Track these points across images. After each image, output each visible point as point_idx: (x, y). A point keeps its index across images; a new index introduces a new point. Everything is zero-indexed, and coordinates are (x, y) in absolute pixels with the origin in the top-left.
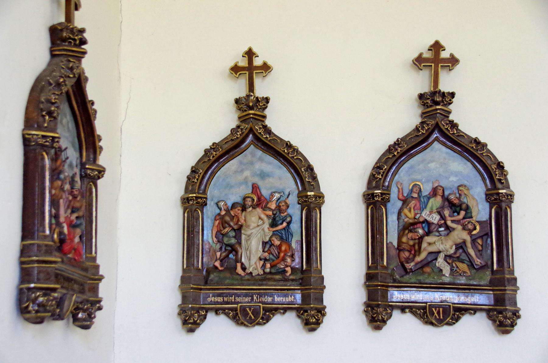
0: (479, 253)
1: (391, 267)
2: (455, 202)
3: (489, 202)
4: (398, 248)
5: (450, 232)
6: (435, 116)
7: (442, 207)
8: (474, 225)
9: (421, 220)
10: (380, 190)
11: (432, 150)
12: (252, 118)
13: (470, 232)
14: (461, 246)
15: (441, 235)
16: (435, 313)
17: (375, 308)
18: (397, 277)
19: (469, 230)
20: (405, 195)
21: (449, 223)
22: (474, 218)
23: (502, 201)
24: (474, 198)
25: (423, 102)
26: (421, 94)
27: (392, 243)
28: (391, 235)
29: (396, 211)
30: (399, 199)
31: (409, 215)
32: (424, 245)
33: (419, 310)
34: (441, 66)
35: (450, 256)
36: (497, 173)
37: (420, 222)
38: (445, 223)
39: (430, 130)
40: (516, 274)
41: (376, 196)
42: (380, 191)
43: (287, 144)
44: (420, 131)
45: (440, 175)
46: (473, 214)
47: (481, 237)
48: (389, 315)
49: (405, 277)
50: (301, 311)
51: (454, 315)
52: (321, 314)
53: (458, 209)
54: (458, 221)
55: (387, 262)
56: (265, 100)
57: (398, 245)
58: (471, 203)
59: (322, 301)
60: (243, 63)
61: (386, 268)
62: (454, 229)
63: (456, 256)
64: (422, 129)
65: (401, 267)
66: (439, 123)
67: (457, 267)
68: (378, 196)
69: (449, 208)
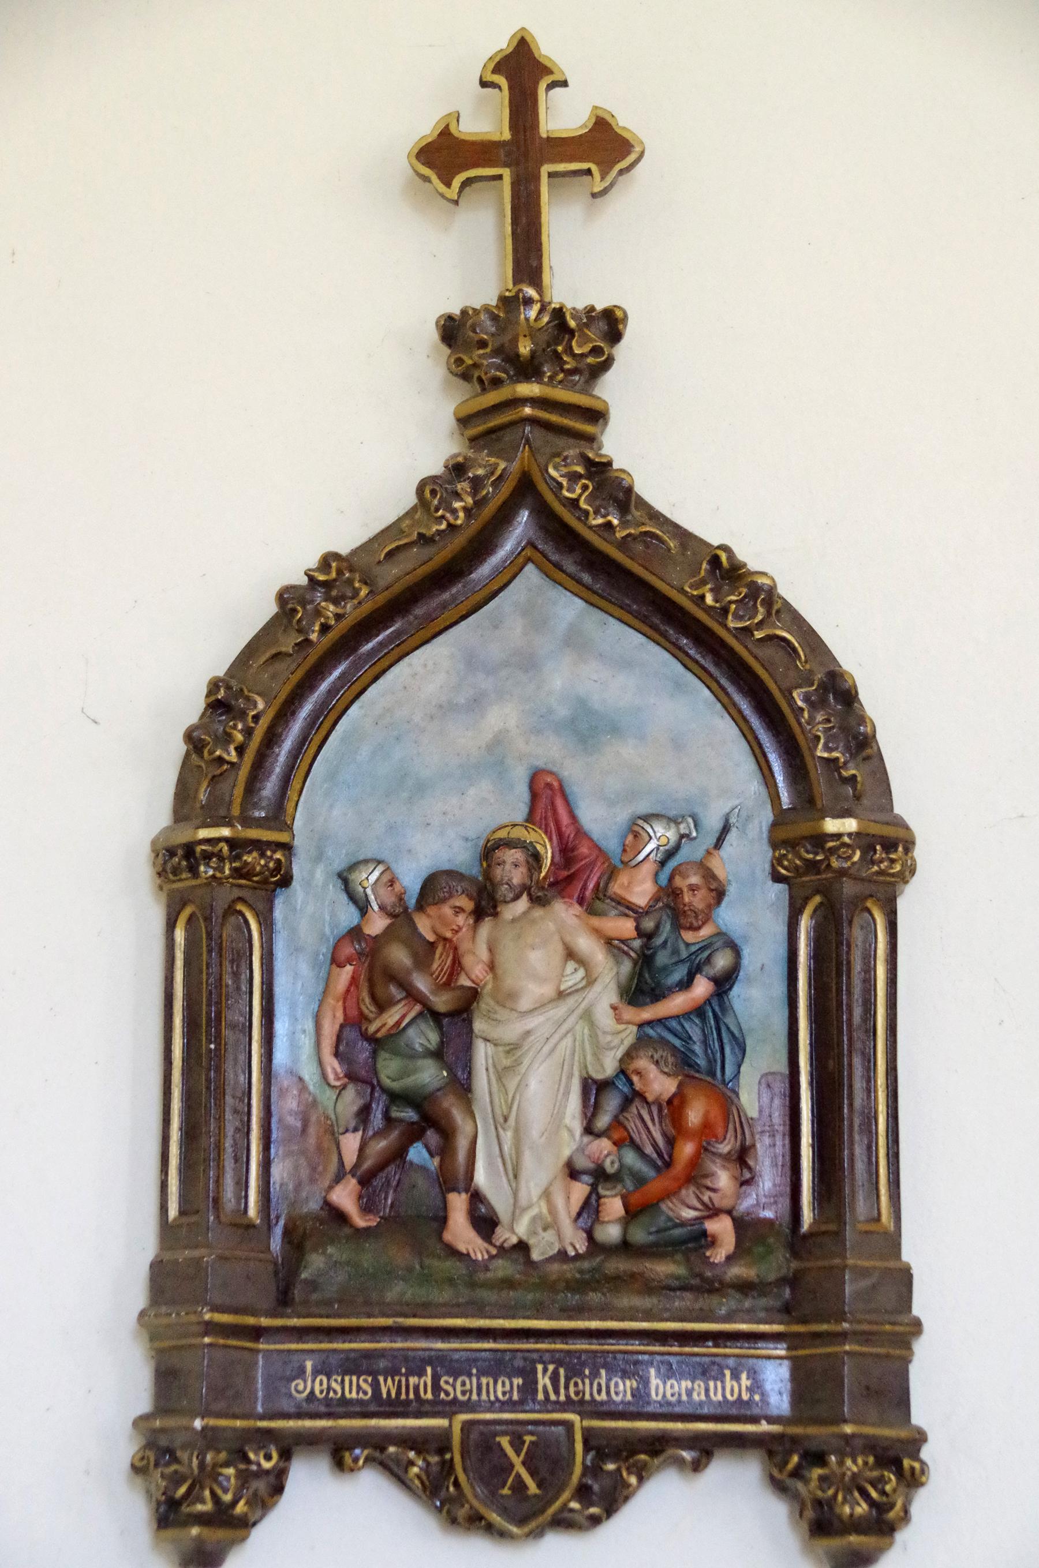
12: (533, 421)
25: (459, 361)
26: (450, 318)
34: (551, 175)
39: (489, 510)
43: (715, 561)
50: (791, 1459)
52: (900, 1473)
56: (603, 325)
59: (900, 1400)
60: (485, 120)
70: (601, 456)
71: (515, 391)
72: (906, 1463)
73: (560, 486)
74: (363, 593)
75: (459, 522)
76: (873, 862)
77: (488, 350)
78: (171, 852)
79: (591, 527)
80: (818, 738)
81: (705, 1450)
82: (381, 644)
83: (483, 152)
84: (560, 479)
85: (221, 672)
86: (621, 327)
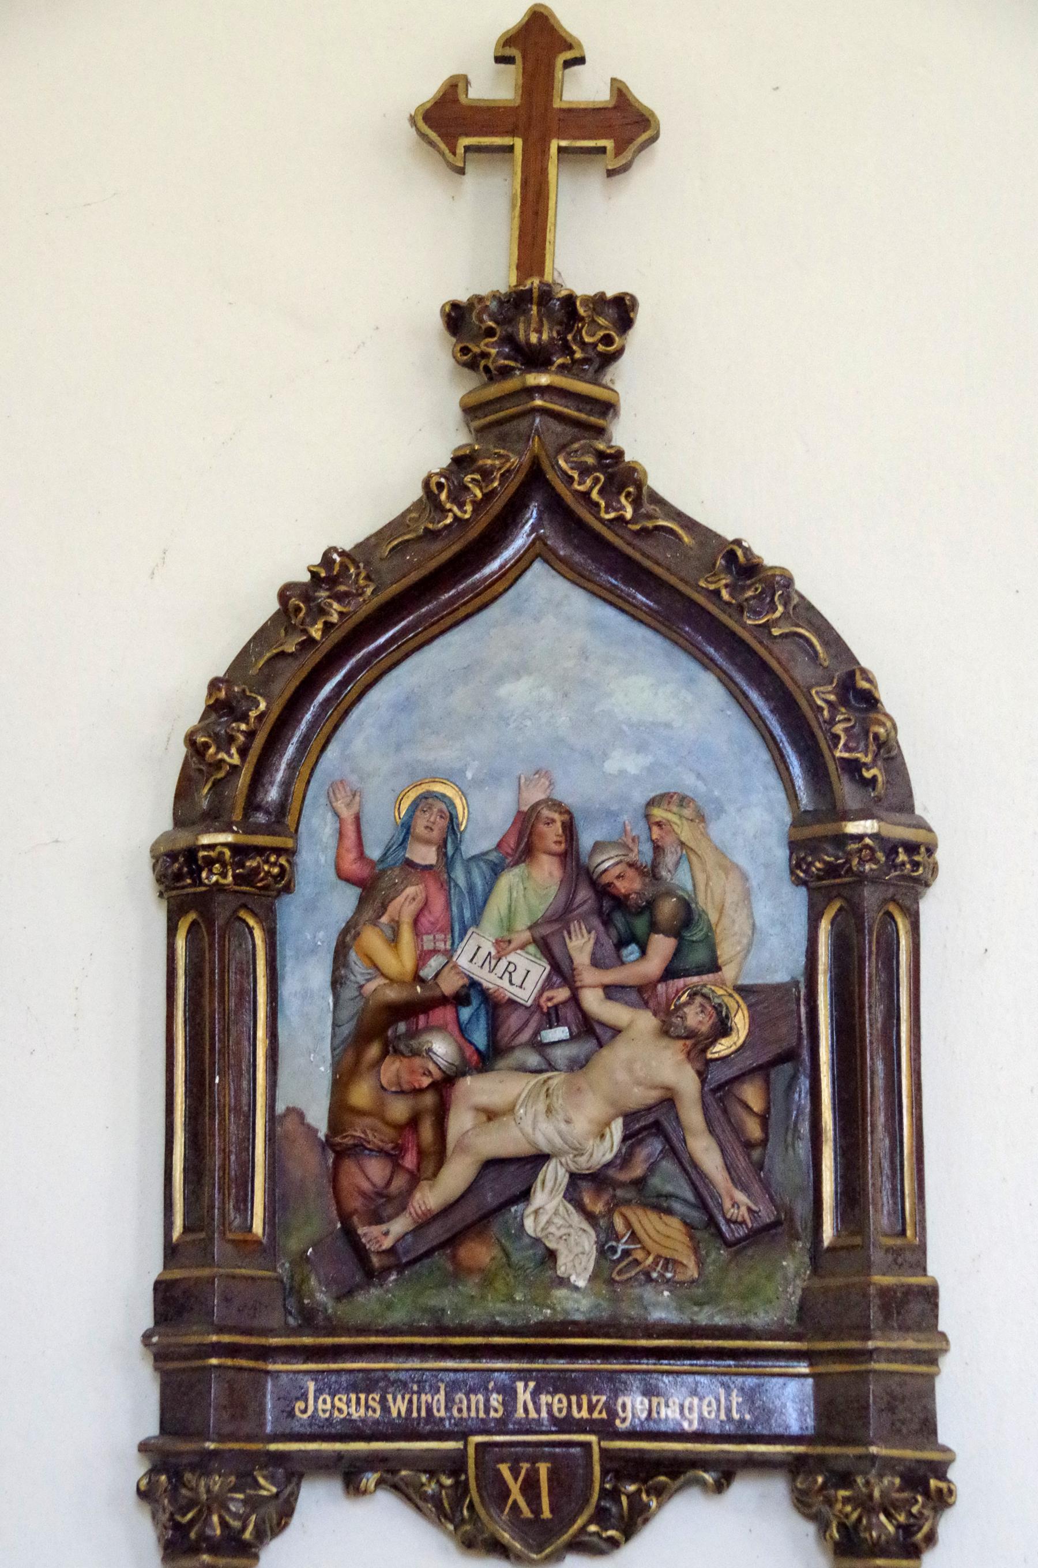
0: (749, 1158)
1: (294, 1244)
2: (622, 887)
3: (804, 883)
4: (329, 1144)
5: (601, 1045)
6: (523, 425)
7: (562, 917)
8: (718, 1008)
9: (449, 985)
10: (227, 828)
11: (517, 611)
13: (697, 1045)
15: (551, 1067)
16: (515, 1488)
17: (188, 1476)
18: (321, 1297)
19: (691, 1034)
20: (374, 853)
21: (593, 1001)
22: (729, 973)
23: (861, 878)
24: (728, 866)
25: (465, 350)
26: (455, 306)
27: (301, 1115)
28: (303, 1076)
29: (327, 939)
30: (341, 875)
31: (391, 959)
32: (461, 1121)
33: (432, 1474)
34: (560, 149)
35: (597, 1179)
36: (839, 729)
37: (443, 1000)
38: (575, 999)
39: (497, 506)
40: (938, 1266)
41: (210, 862)
42: (228, 838)
43: (731, 556)
44: (444, 511)
46: (725, 951)
47: (763, 1070)
48: (271, 1511)
49: (360, 1298)
51: (614, 1495)
52: (927, 1494)
53: (640, 925)
54: (640, 989)
55: (270, 1220)
58: (713, 894)
59: (928, 1427)
60: (493, 86)
61: (267, 1250)
62: (616, 1031)
63: (624, 1176)
64: (454, 498)
65: (341, 1244)
66: (545, 464)
67: (634, 1237)
68: (220, 859)
69: (596, 922)
70: (612, 447)
71: (524, 382)
72: (933, 1483)
73: (571, 478)
74: (369, 591)
75: (467, 516)
76: (895, 867)
77: (495, 339)
78: (173, 856)
79: (602, 521)
80: (837, 738)
81: (726, 1474)
82: (313, 725)
83: (488, 118)
84: (570, 472)
85: (221, 673)
86: (632, 315)
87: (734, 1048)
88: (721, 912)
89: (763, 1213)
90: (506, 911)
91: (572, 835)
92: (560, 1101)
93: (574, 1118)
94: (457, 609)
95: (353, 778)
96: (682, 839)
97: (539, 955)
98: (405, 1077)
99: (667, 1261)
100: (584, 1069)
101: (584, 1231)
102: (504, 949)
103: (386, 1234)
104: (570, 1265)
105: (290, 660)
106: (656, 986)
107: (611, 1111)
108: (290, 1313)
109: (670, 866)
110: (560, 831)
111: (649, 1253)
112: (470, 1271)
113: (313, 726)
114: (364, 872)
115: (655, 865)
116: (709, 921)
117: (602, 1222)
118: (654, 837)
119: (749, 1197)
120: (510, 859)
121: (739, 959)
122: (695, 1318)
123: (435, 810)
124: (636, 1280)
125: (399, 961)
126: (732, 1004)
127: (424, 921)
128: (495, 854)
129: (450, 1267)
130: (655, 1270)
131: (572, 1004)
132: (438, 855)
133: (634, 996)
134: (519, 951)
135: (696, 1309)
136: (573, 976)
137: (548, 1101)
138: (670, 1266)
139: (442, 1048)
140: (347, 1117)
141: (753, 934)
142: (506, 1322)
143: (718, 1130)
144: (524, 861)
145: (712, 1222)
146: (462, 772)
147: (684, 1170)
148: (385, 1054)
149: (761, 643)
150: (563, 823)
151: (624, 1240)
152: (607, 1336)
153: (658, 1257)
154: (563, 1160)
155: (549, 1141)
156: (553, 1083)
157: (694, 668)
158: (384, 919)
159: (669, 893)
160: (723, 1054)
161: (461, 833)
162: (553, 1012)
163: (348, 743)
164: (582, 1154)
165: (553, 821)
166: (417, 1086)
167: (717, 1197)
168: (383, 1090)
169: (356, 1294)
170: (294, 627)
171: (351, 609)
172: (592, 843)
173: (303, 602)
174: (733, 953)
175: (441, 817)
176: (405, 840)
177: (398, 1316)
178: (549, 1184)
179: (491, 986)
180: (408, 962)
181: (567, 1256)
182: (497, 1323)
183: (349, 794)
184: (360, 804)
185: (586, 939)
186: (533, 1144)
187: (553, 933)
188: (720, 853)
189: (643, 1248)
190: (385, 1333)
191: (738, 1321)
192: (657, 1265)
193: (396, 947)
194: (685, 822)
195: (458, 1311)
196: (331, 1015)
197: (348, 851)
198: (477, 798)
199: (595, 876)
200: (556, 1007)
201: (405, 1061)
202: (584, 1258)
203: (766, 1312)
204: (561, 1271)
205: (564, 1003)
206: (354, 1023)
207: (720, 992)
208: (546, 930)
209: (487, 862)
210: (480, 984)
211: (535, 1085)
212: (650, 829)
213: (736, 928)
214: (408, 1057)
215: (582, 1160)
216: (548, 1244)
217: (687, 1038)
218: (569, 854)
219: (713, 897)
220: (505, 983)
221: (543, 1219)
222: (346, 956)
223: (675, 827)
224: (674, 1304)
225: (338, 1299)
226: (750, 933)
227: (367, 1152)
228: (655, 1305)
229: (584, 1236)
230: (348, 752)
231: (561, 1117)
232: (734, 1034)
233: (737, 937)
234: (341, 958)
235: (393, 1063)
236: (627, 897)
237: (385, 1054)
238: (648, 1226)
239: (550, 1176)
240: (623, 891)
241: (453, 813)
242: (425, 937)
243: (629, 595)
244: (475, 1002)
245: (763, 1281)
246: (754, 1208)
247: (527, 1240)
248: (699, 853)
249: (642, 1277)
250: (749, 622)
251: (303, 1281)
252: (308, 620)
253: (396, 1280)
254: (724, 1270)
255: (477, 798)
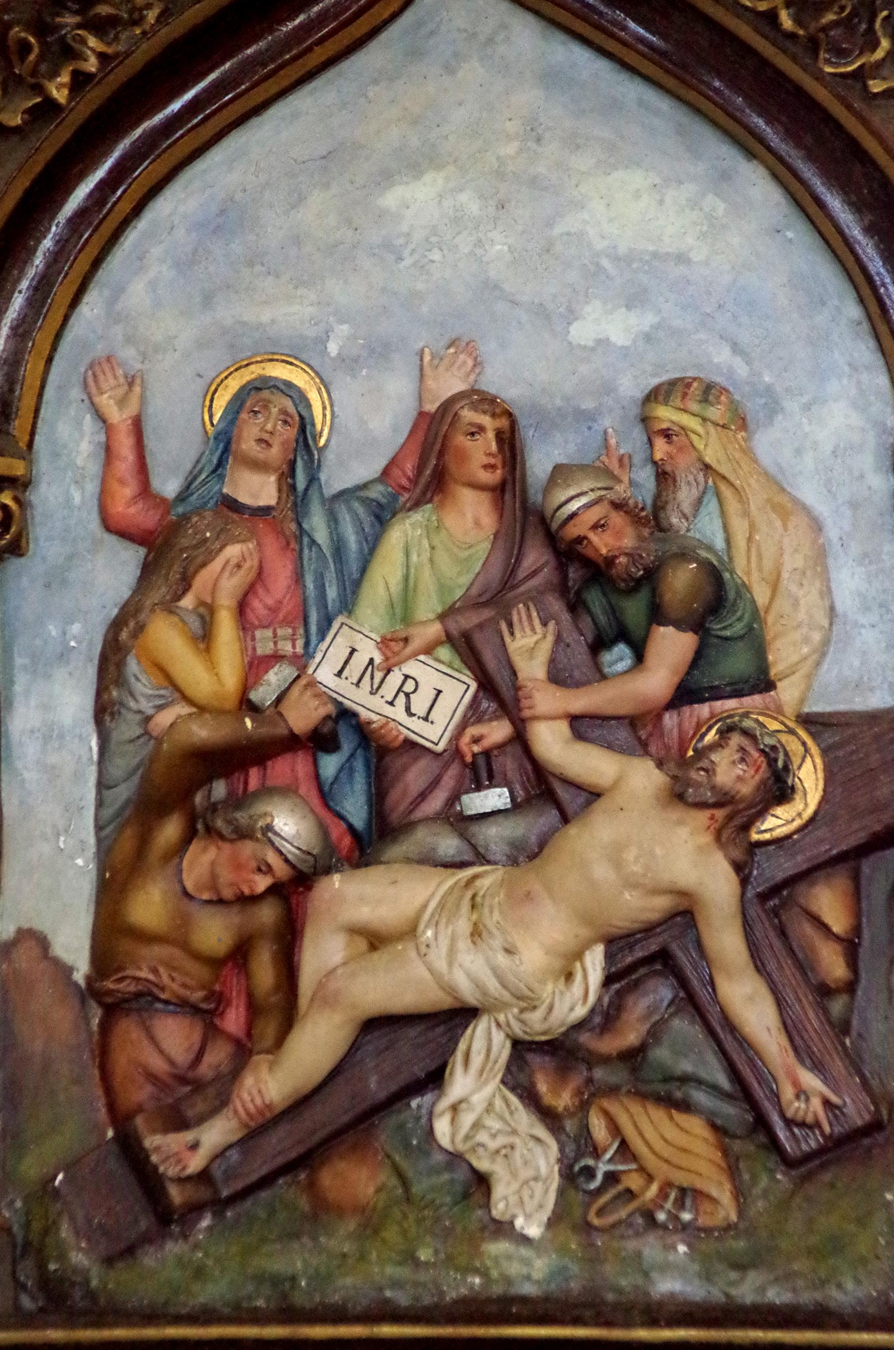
2: (602, 544)
4: (92, 991)
5: (565, 819)
7: (497, 597)
8: (770, 754)
9: (302, 716)
13: (734, 820)
14: (653, 954)
15: (481, 858)
18: (78, 1258)
19: (724, 800)
20: (169, 486)
21: (552, 742)
22: (788, 693)
24: (787, 506)
27: (42, 942)
29: (85, 635)
30: (109, 525)
31: (200, 673)
32: (323, 952)
35: (561, 1051)
37: (291, 743)
38: (520, 739)
45: (490, 288)
46: (783, 655)
49: (149, 1259)
53: (634, 609)
54: (633, 721)
57: (104, 958)
62: (593, 795)
63: (609, 1045)
65: (114, 1164)
69: (556, 605)
74: (151, 16)
82: (56, 258)
87: (797, 823)
88: (775, 587)
89: (850, 1109)
90: (401, 587)
91: (514, 456)
92: (496, 916)
93: (519, 944)
94: (309, 49)
95: (128, 354)
96: (708, 460)
97: (457, 663)
98: (226, 876)
99: (683, 1191)
100: (537, 861)
101: (538, 1140)
102: (396, 654)
103: (194, 1146)
104: (513, 1199)
105: (15, 139)
106: (659, 717)
107: (585, 932)
108: (23, 1287)
109: (687, 508)
110: (494, 447)
111: (650, 1178)
112: (340, 1211)
113: (55, 261)
114: (142, 516)
115: (659, 506)
116: (753, 601)
117: (570, 1126)
118: (658, 456)
119: (825, 1081)
120: (407, 496)
121: (805, 669)
122: (733, 1292)
123: (275, 411)
124: (630, 1225)
125: (214, 674)
126: (793, 746)
127: (258, 607)
128: (380, 488)
129: (304, 1203)
130: (662, 1207)
131: (518, 749)
132: (280, 491)
133: (623, 734)
134: (422, 657)
135: (733, 1275)
136: (518, 700)
137: (475, 917)
138: (688, 1202)
139: (290, 825)
140: (126, 945)
141: (831, 624)
142: (402, 1299)
143: (772, 966)
144: (430, 501)
145: (761, 1123)
146: (321, 342)
147: (711, 1032)
148: (189, 836)
149: (849, 107)
150: (499, 435)
151: (608, 1156)
152: (577, 1321)
153: (667, 1185)
154: (501, 1018)
155: (479, 985)
156: (484, 883)
157: (725, 153)
158: (188, 602)
159: (684, 555)
160: (779, 832)
161: (321, 450)
162: (481, 762)
163: (119, 290)
164: (535, 1008)
165: (481, 429)
166: (247, 891)
167: (767, 1079)
168: (187, 897)
169: (140, 1251)
170: (20, 80)
171: (121, 48)
172: (550, 469)
173: (35, 35)
174: (794, 658)
175: (285, 422)
176: (221, 464)
177: (212, 1292)
178: (477, 1060)
179: (374, 717)
180: (230, 675)
181: (509, 1184)
182: (387, 1301)
183: (122, 380)
184: (143, 399)
185: (539, 636)
186: (450, 990)
187: (480, 626)
188: (775, 483)
189: (642, 1169)
190: (192, 1319)
191: (807, 1297)
192: (666, 1197)
193: (208, 650)
194: (712, 429)
195: (320, 1279)
196: (94, 769)
197: (122, 482)
198: (348, 391)
199: (554, 526)
200: (487, 754)
201: (227, 847)
202: (539, 1187)
203: (858, 1282)
204: (499, 1209)
205: (501, 746)
206: (136, 779)
207: (773, 725)
208: (468, 621)
209: (365, 501)
210: (355, 715)
211: (452, 889)
212: (650, 442)
213: (802, 616)
214: (232, 841)
215: (535, 1018)
216: (475, 1163)
217: (718, 805)
218: (509, 487)
219: (760, 557)
220: (398, 713)
221: (467, 1119)
222: (121, 665)
223: (694, 437)
224: (696, 1267)
225: (109, 1261)
226: (826, 623)
227: (159, 1006)
228: (665, 1268)
229: (538, 1150)
230: (119, 307)
231: (497, 943)
232: (798, 797)
233: (804, 630)
234: (112, 668)
235: (205, 850)
236: (610, 561)
237: (189, 836)
238: (650, 1133)
239: (478, 1045)
240: (604, 551)
241: (304, 413)
242: (258, 634)
243: (615, 23)
244: (348, 743)
245: (852, 1228)
246: (834, 1099)
247: (438, 1158)
248: (737, 483)
249: (640, 1221)
250: (829, 69)
251: (46, 1231)
252: (43, 67)
253: (210, 1228)
254: (784, 1205)
255: (348, 391)
